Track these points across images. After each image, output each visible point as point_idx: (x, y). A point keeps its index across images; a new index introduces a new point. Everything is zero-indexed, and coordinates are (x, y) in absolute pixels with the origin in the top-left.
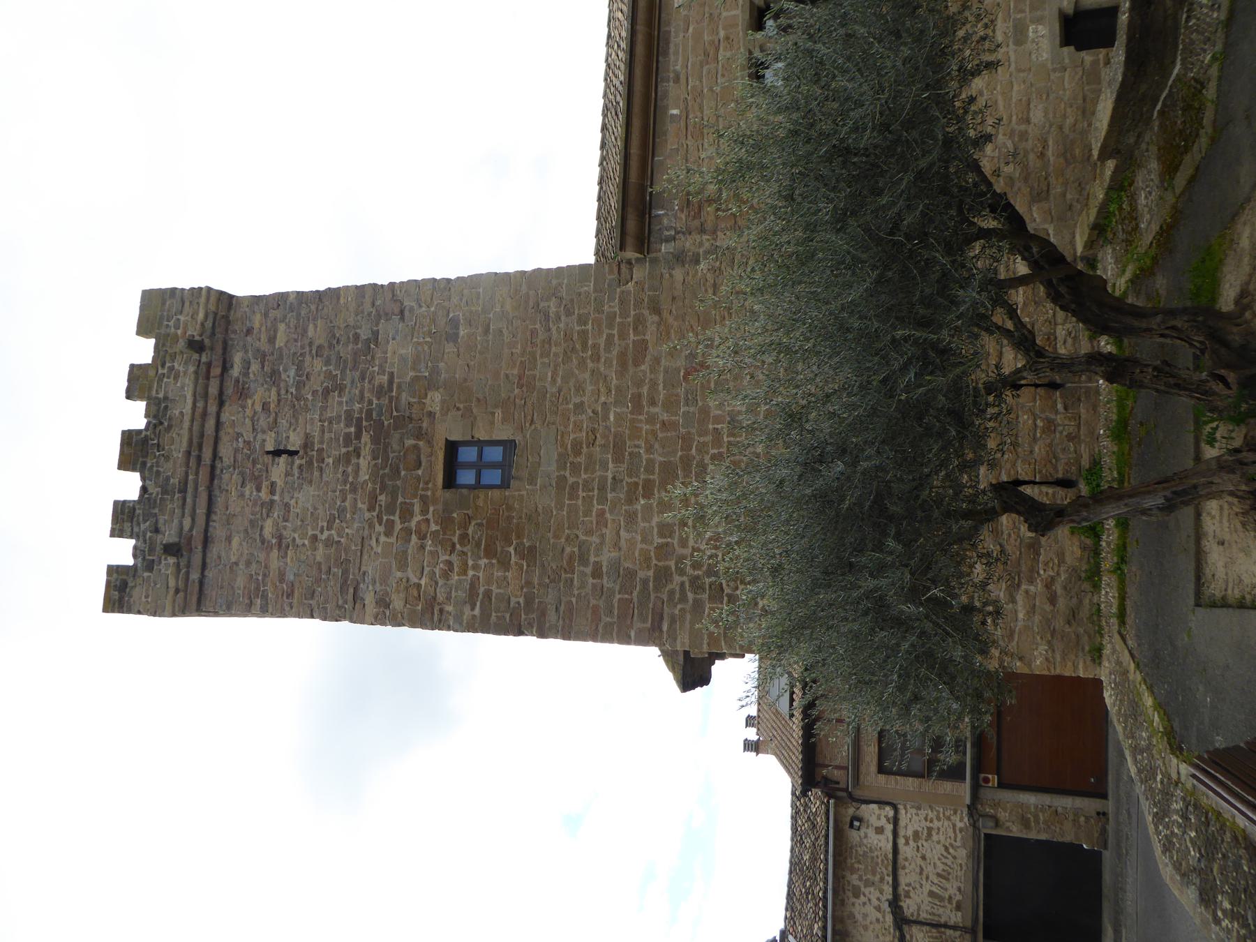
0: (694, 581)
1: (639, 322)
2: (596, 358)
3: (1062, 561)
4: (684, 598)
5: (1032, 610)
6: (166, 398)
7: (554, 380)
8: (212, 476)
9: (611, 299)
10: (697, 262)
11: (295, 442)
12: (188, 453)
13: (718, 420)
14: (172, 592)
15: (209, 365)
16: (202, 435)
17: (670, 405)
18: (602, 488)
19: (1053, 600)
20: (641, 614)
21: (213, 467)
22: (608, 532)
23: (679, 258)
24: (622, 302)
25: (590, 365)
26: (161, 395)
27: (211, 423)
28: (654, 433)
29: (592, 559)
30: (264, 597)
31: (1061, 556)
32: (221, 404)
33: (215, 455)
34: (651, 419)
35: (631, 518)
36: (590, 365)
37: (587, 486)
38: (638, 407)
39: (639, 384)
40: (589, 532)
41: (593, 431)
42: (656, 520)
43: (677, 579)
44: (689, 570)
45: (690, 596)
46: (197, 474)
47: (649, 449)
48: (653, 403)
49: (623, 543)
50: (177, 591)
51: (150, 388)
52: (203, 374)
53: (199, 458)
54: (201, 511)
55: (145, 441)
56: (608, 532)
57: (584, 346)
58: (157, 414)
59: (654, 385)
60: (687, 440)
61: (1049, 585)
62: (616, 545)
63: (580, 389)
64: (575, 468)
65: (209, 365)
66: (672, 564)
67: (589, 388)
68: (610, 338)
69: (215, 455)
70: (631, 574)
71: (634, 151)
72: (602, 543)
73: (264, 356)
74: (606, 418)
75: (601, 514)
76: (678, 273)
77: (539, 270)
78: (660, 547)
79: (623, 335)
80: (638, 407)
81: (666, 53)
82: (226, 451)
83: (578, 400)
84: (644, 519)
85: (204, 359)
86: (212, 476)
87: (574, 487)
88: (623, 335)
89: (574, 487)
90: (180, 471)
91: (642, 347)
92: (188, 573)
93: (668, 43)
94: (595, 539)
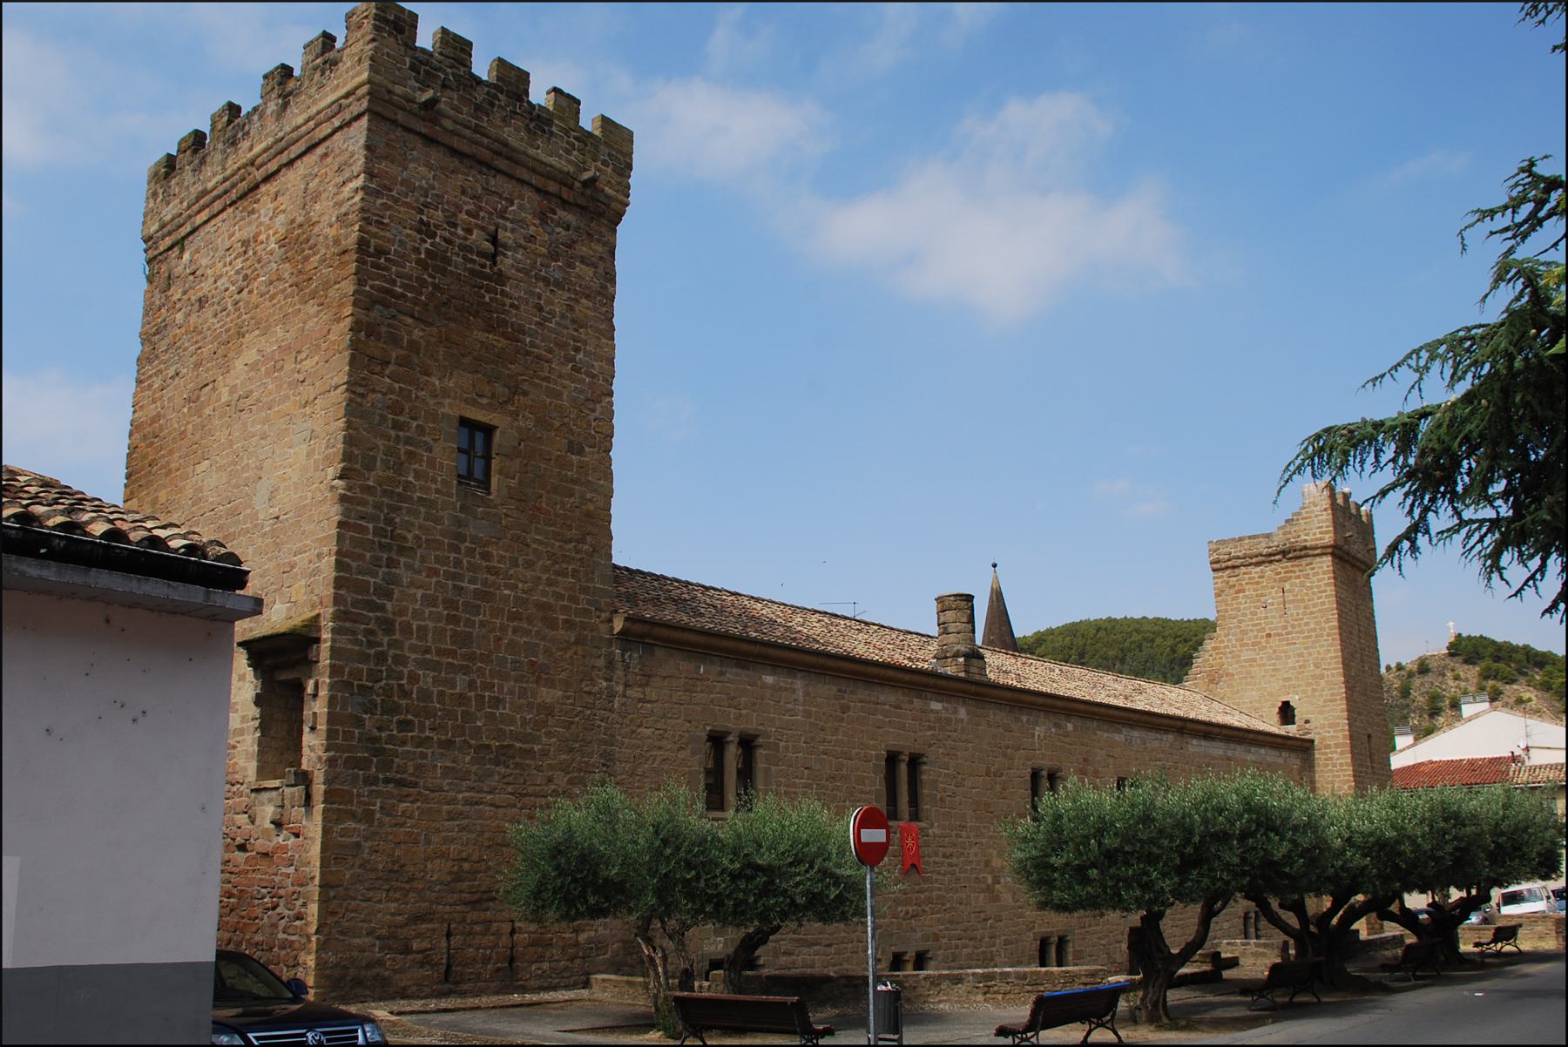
0: (381, 657)
1: (569, 624)
2: (550, 583)
3: (395, 971)
4: (370, 644)
5: (362, 950)
6: (552, 133)
7: (536, 541)
8: (481, 163)
9: (589, 602)
10: (606, 680)
11: (506, 263)
12: (506, 145)
13: (501, 687)
14: (390, 86)
15: (571, 187)
16: (517, 163)
17: (512, 646)
18: (454, 577)
19: (369, 966)
20: (358, 601)
21: (489, 167)
22: (422, 577)
23: (610, 664)
24: (585, 610)
25: (545, 577)
26: (554, 129)
27: (526, 176)
28: (493, 630)
29: (402, 560)
30: (378, 194)
31: (401, 971)
32: (538, 190)
33: (499, 171)
34: (503, 628)
35: (431, 601)
36: (545, 577)
37: (458, 563)
38: (515, 617)
39: (530, 621)
40: (423, 559)
41: (497, 574)
42: (431, 625)
43: (386, 640)
44: (392, 652)
45: (372, 652)
46: (488, 148)
47: (482, 624)
48: (515, 631)
49: (413, 591)
50: (390, 92)
51: (561, 119)
52: (565, 180)
53: (498, 153)
54: (455, 143)
55: (520, 99)
56: (422, 577)
57: (557, 573)
58: (538, 120)
59: (527, 633)
60: (486, 658)
61: (380, 963)
62: (412, 584)
63: (529, 565)
64: (470, 552)
65: (571, 187)
66: (397, 636)
67: (529, 574)
68: (561, 597)
69: (499, 171)
70: (388, 595)
71: (686, 636)
72: (415, 572)
73: (569, 246)
74: (507, 587)
75: (436, 573)
76: (601, 662)
77: (611, 538)
78: (409, 625)
79: (565, 609)
80: (515, 617)
81: (737, 666)
82: (497, 183)
83: (520, 561)
84: (431, 613)
85: (577, 184)
86: (481, 163)
87: (457, 549)
88: (565, 609)
89: (457, 549)
90: (492, 131)
91: (553, 624)
92: (403, 109)
93: (743, 668)
94: (417, 564)
